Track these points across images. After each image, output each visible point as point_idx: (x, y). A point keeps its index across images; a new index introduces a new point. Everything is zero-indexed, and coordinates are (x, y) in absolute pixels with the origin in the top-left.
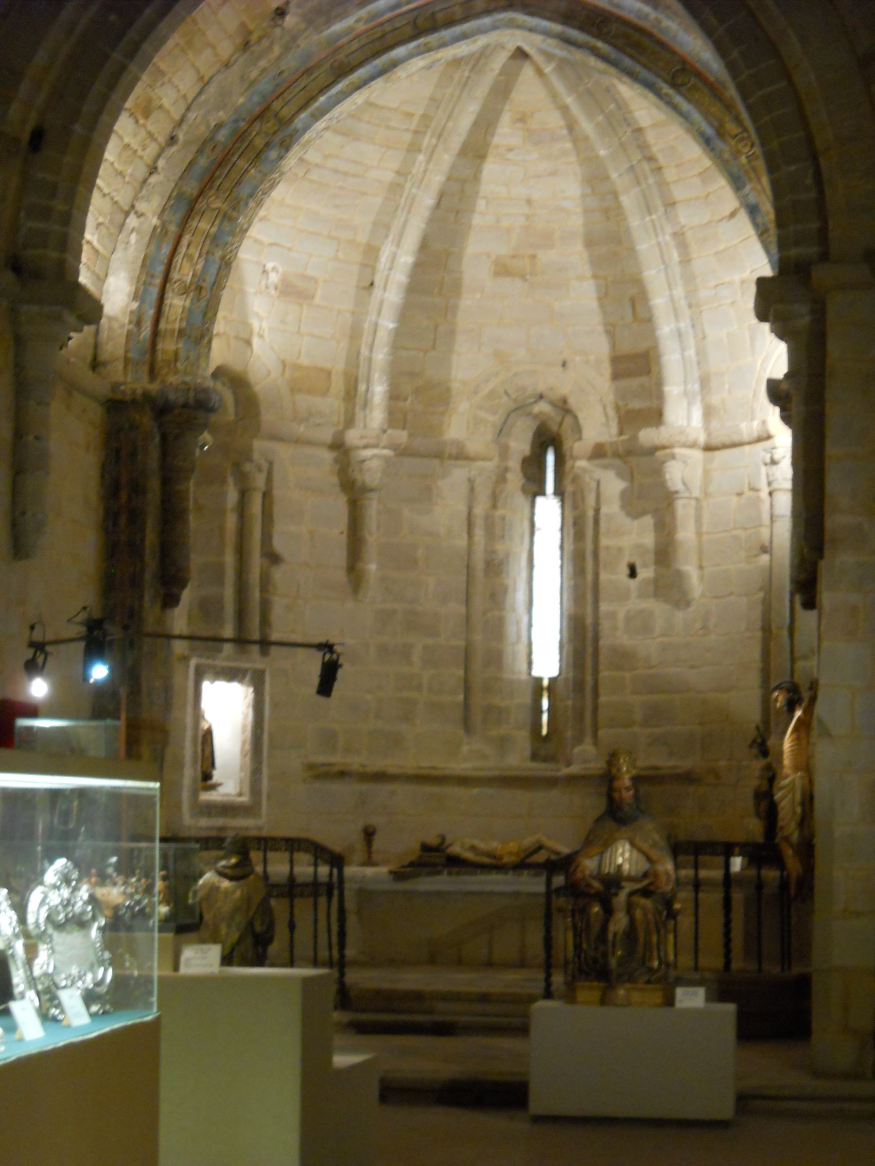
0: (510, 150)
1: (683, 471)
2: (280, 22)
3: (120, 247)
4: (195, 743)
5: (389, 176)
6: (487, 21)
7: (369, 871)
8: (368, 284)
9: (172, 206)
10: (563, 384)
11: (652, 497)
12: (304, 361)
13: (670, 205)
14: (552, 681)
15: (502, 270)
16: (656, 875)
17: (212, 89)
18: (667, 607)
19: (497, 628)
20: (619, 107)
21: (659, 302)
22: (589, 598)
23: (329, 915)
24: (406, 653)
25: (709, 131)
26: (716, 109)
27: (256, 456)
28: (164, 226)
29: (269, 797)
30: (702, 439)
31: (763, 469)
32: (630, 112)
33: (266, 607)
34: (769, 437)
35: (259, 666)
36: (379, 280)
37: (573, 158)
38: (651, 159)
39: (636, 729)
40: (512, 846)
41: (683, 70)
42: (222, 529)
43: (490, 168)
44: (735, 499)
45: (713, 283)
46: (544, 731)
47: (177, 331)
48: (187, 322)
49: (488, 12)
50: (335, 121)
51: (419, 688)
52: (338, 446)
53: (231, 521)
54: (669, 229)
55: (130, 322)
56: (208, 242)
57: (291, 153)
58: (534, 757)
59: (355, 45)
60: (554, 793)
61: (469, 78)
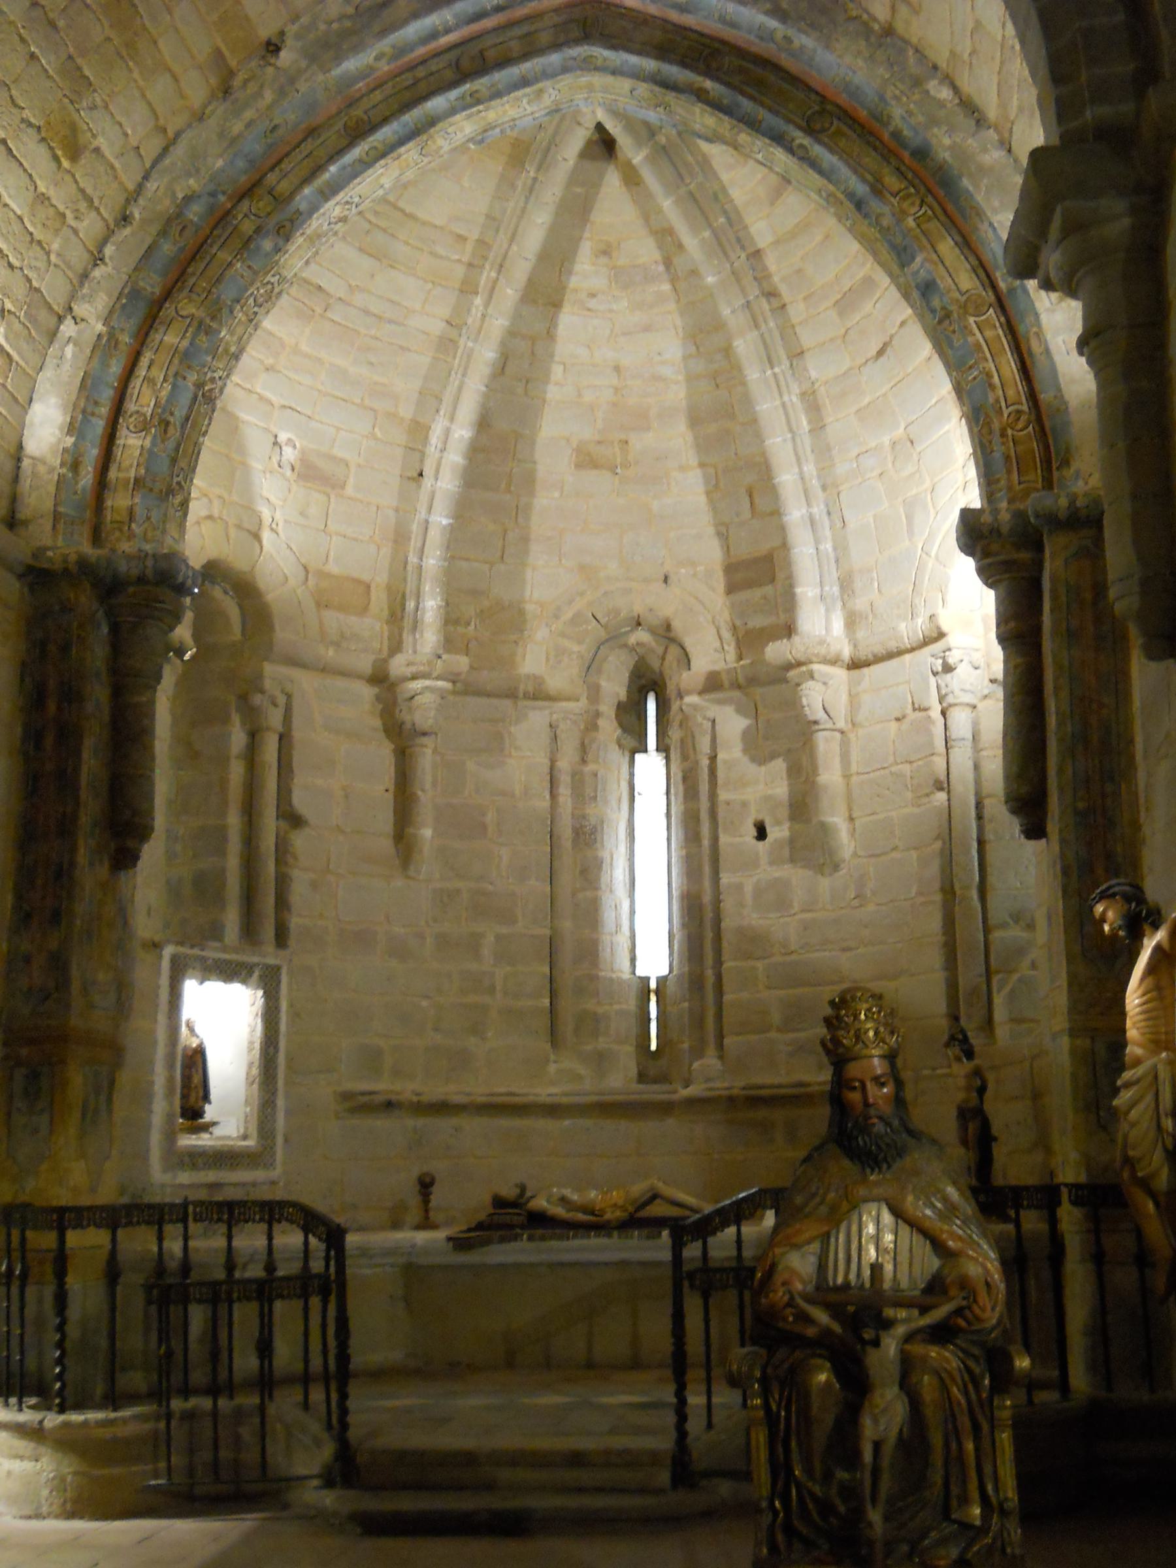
0: (593, 295)
1: (825, 694)
2: (272, 61)
3: (50, 362)
4: (171, 1066)
5: (436, 327)
6: (555, 58)
7: (421, 1237)
8: (415, 475)
9: (124, 306)
10: (665, 604)
11: (786, 734)
12: (333, 568)
13: (797, 354)
14: (662, 981)
15: (587, 460)
16: (964, 1284)
17: (179, 151)
18: (809, 873)
19: (590, 913)
20: (730, 223)
21: (786, 479)
22: (707, 869)
23: (324, 1326)
24: (473, 945)
25: (861, 189)
26: (871, 160)
27: (268, 684)
28: (111, 334)
29: (286, 1141)
30: (846, 653)
31: (933, 680)
32: (746, 227)
33: (282, 883)
34: (941, 635)
35: (271, 961)
36: (428, 471)
37: (672, 306)
38: (771, 294)
39: (773, 1034)
40: (616, 1196)
41: (822, 112)
42: (223, 783)
43: (567, 320)
44: (894, 725)
45: (854, 453)
46: (653, 1047)
47: (132, 481)
48: (147, 470)
49: (556, 46)
50: (354, 210)
51: (492, 990)
52: (380, 678)
53: (237, 772)
54: (795, 389)
55: (62, 465)
56: (176, 361)
57: (292, 247)
58: (642, 1077)
59: (378, 96)
60: (671, 1122)
61: (535, 179)
